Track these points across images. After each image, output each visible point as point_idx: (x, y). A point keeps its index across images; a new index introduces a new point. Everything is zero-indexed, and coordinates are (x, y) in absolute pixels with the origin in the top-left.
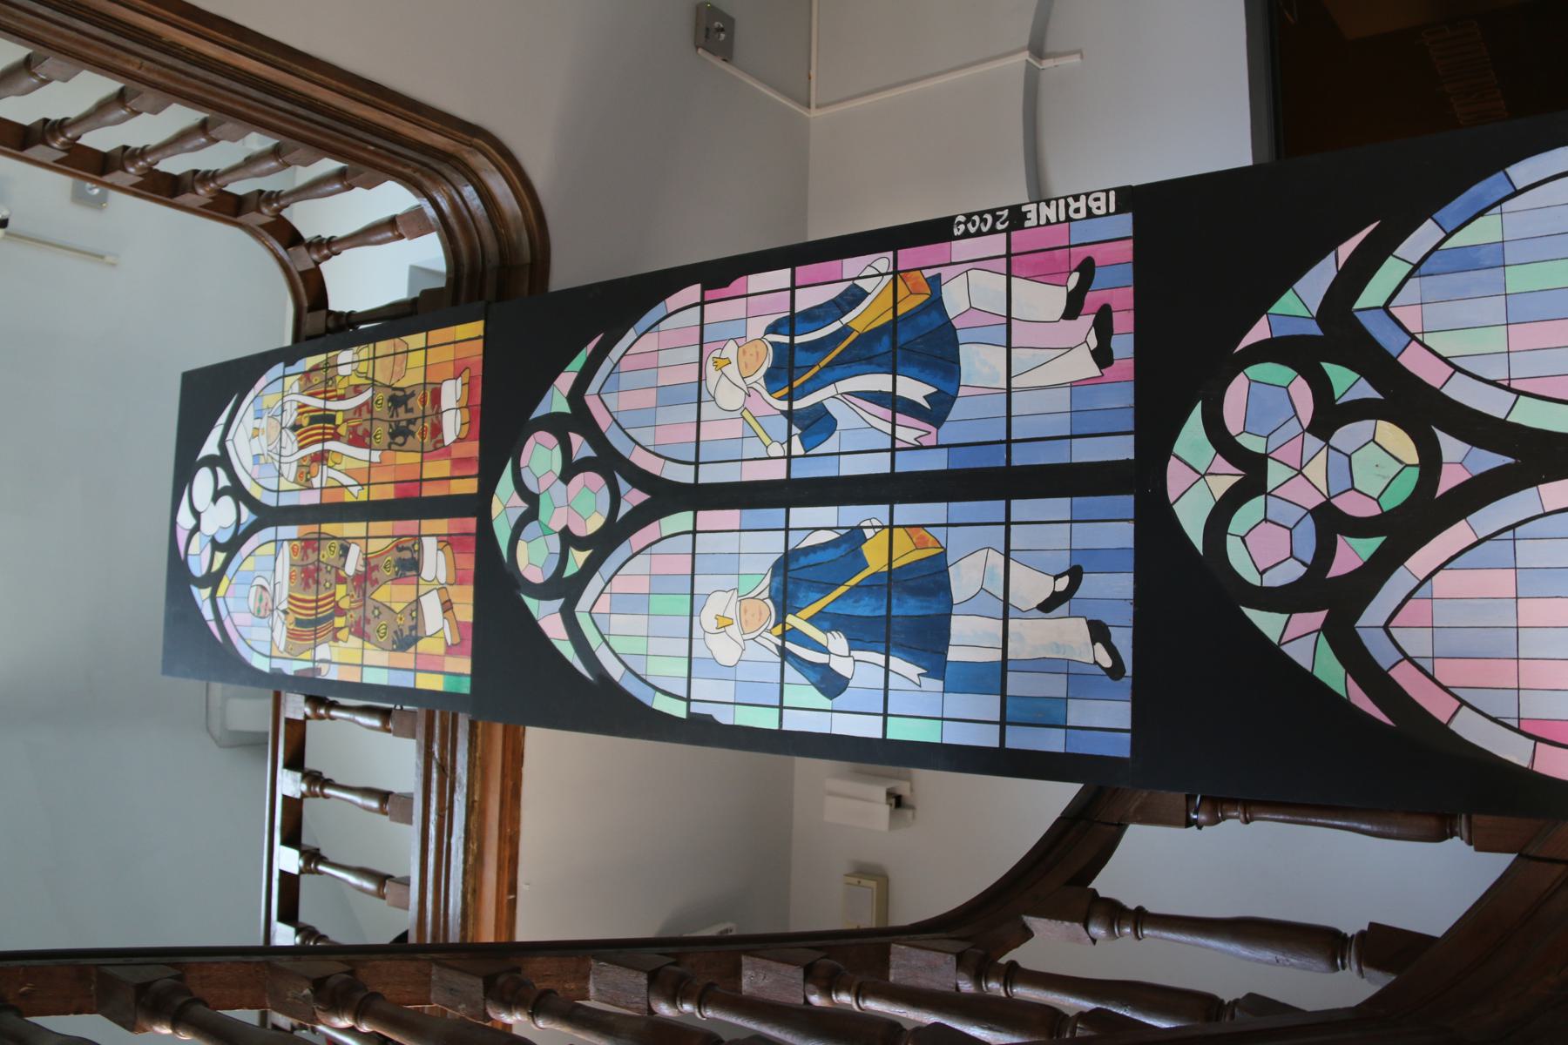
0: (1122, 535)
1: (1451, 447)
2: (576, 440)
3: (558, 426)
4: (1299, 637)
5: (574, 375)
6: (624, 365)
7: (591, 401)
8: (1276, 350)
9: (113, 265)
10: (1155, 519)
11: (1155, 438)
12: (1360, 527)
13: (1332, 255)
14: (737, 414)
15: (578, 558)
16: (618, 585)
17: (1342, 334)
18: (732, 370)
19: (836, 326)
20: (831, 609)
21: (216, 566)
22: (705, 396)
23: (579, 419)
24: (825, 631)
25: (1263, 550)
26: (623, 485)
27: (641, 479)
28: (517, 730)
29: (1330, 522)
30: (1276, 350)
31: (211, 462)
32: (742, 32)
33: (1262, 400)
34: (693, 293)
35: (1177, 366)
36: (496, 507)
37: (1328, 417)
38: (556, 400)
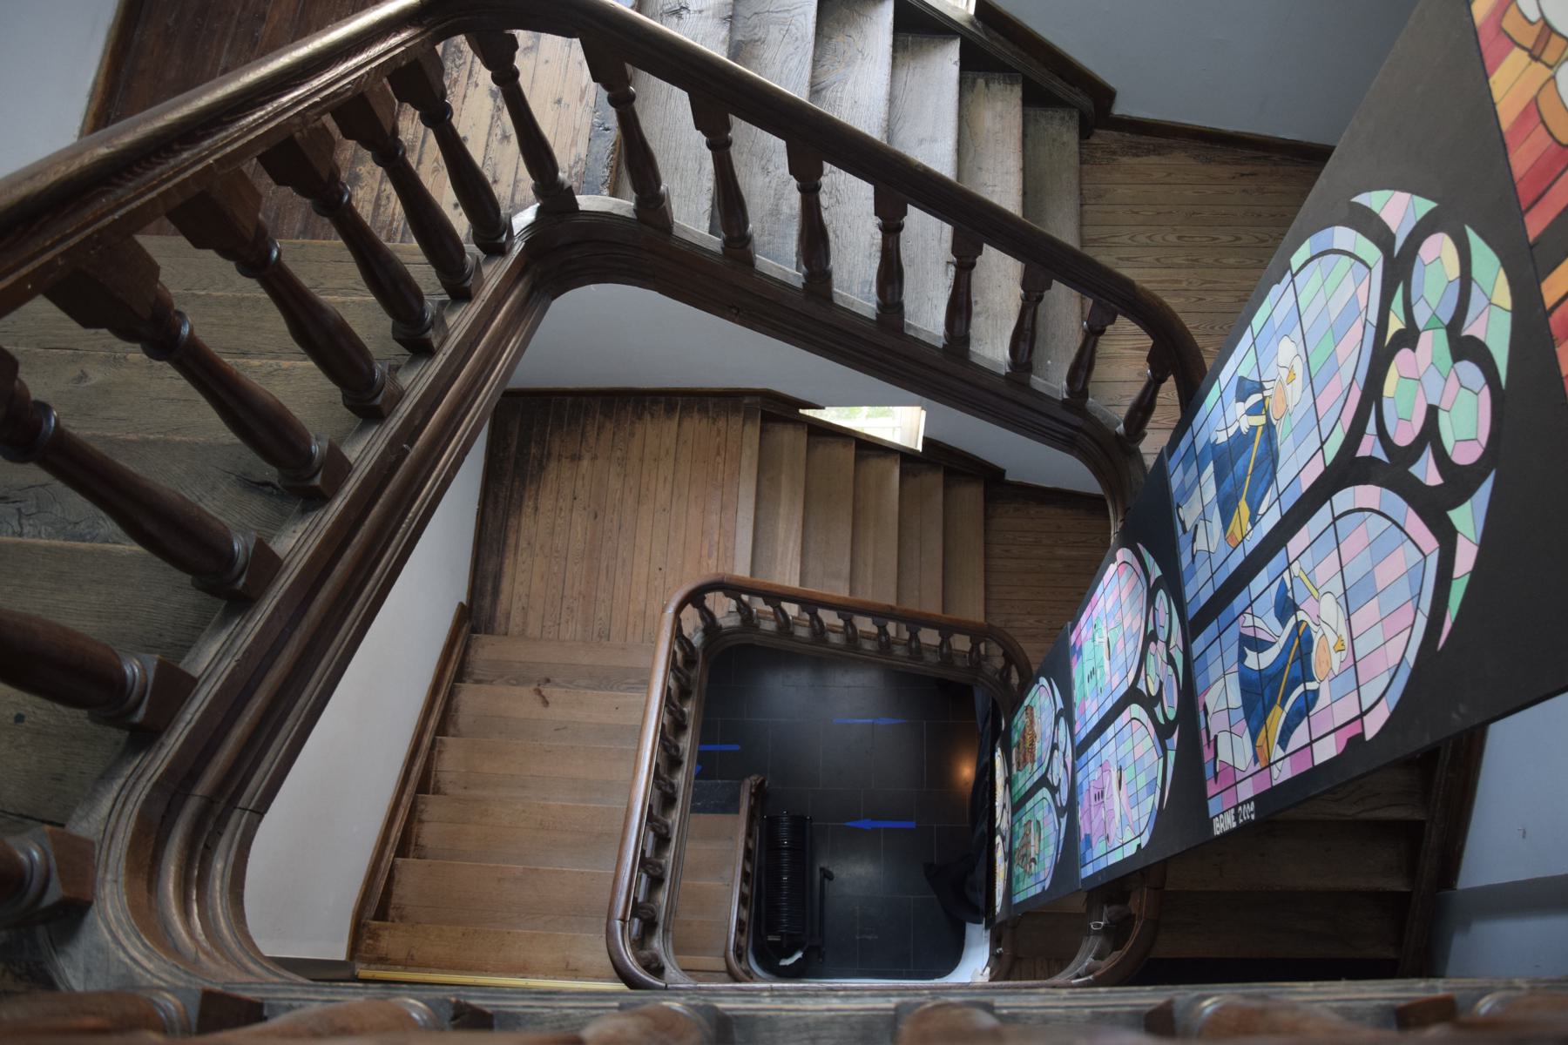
4: (1399, 209)
5: (1456, 574)
6: (1410, 607)
13: (1283, 552)
14: (1322, 591)
15: (1396, 324)
16: (1358, 325)
18: (1332, 639)
19: (1287, 708)
20: (1245, 455)
22: (1342, 600)
23: (1434, 509)
24: (905, 1004)
26: (1380, 454)
28: (728, 634)
31: (1459, 482)
32: (1392, 1034)
36: (1502, 294)
38: (1468, 519)
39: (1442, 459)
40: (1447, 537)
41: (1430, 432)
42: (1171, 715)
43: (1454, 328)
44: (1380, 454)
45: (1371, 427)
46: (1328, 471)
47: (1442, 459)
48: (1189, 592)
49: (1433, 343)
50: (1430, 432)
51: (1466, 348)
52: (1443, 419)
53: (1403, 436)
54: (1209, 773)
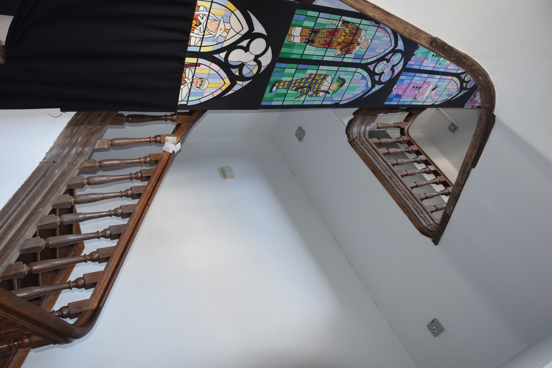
0: (283, 50)
1: (372, 69)
2: (377, 79)
3: (242, 78)
4: (259, 28)
7: (370, 86)
8: (382, 83)
9: (160, 142)
10: (405, 63)
11: (271, 67)
12: (242, 47)
15: (387, 57)
17: (233, 79)
21: (390, 55)
23: (374, 83)
25: (258, 45)
27: (217, 62)
29: (246, 49)
30: (382, 83)
31: (379, 83)
33: (250, 70)
34: (341, 103)
35: (262, 79)
36: (400, 69)
37: (241, 66)
38: (377, 87)
39: (380, 79)
40: (373, 86)
41: (381, 74)
42: (468, 87)
43: (393, 66)
44: (463, 78)
45: (465, 74)
46: (456, 74)
47: (380, 79)
48: (409, 63)
49: (390, 65)
50: (381, 74)
51: (392, 70)
52: (383, 75)
53: (466, 80)
54: (470, 99)
